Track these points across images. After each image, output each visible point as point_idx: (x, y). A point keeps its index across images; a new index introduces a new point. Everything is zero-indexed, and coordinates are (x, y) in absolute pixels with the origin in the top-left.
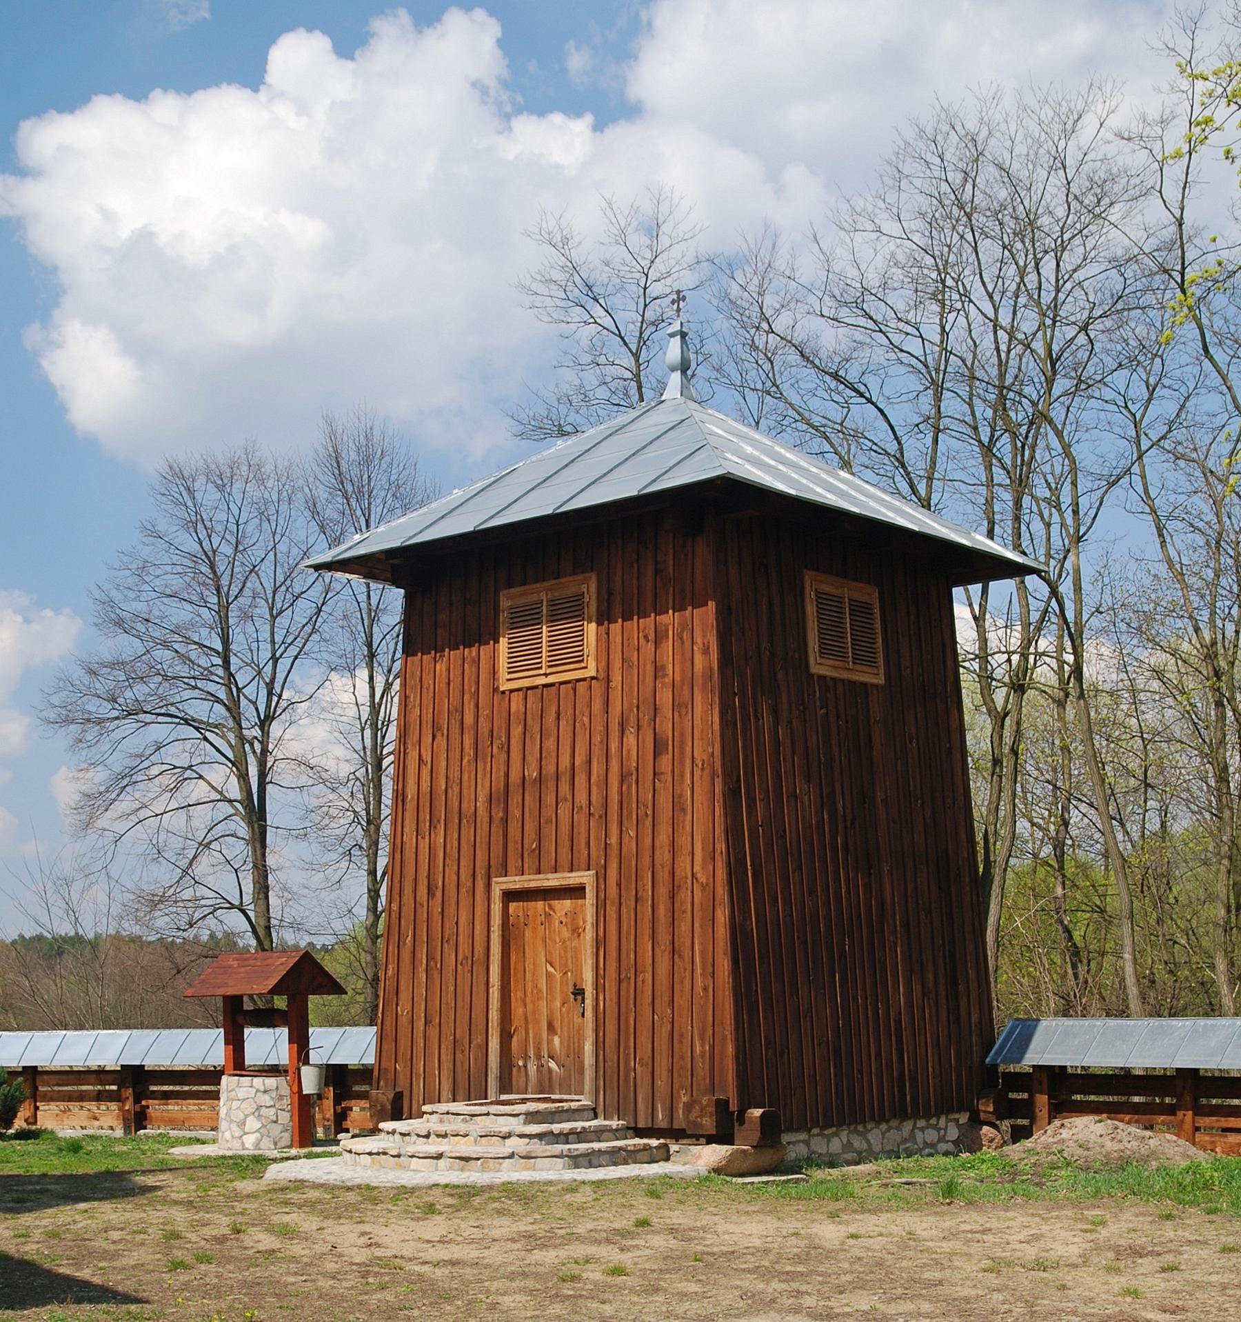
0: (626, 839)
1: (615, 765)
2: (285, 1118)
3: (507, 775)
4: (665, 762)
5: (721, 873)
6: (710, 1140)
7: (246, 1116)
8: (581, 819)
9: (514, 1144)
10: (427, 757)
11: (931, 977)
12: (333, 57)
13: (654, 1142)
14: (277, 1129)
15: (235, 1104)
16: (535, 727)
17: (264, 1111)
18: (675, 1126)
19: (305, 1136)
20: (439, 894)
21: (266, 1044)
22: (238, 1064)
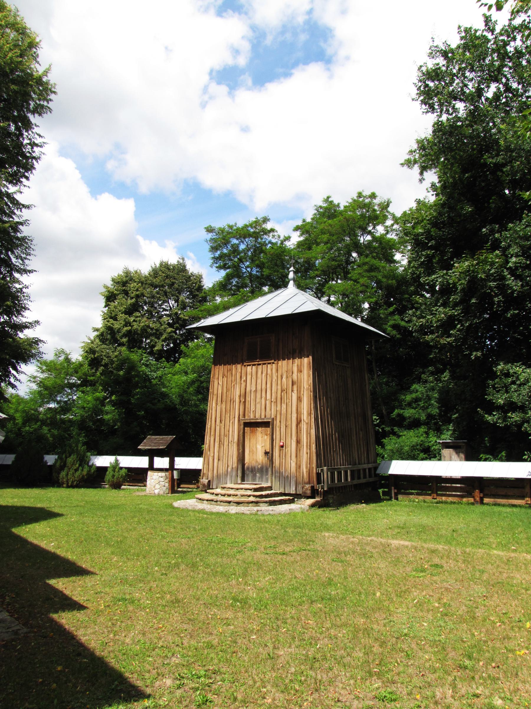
0: (282, 408)
1: (279, 387)
2: (167, 485)
3: (246, 389)
4: (295, 387)
5: (313, 420)
6: (308, 498)
7: (156, 483)
8: (268, 403)
9: (252, 499)
10: (221, 383)
11: (362, 449)
12: (89, 195)
13: (291, 498)
14: (165, 488)
15: (152, 480)
16: (254, 376)
17: (161, 483)
18: (298, 493)
19: (173, 490)
20: (223, 422)
21: (162, 462)
22: (151, 467)
